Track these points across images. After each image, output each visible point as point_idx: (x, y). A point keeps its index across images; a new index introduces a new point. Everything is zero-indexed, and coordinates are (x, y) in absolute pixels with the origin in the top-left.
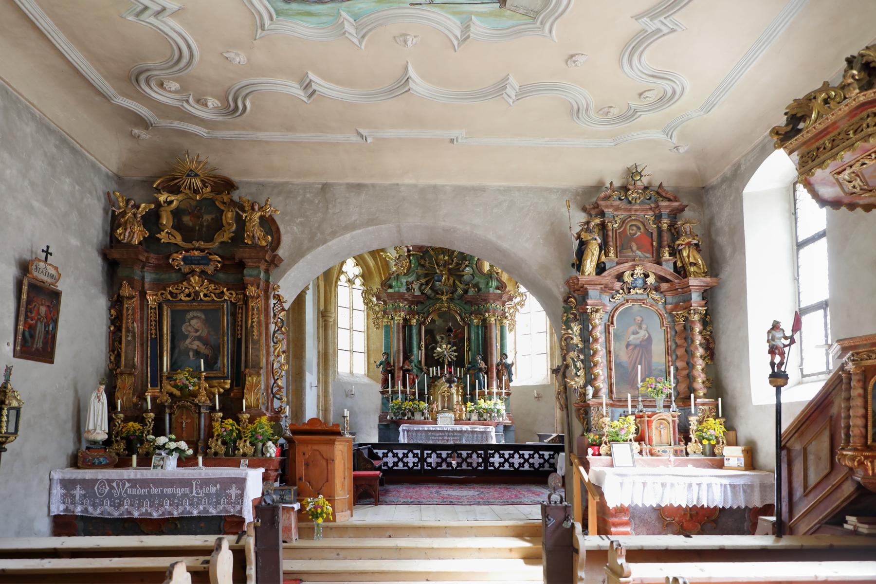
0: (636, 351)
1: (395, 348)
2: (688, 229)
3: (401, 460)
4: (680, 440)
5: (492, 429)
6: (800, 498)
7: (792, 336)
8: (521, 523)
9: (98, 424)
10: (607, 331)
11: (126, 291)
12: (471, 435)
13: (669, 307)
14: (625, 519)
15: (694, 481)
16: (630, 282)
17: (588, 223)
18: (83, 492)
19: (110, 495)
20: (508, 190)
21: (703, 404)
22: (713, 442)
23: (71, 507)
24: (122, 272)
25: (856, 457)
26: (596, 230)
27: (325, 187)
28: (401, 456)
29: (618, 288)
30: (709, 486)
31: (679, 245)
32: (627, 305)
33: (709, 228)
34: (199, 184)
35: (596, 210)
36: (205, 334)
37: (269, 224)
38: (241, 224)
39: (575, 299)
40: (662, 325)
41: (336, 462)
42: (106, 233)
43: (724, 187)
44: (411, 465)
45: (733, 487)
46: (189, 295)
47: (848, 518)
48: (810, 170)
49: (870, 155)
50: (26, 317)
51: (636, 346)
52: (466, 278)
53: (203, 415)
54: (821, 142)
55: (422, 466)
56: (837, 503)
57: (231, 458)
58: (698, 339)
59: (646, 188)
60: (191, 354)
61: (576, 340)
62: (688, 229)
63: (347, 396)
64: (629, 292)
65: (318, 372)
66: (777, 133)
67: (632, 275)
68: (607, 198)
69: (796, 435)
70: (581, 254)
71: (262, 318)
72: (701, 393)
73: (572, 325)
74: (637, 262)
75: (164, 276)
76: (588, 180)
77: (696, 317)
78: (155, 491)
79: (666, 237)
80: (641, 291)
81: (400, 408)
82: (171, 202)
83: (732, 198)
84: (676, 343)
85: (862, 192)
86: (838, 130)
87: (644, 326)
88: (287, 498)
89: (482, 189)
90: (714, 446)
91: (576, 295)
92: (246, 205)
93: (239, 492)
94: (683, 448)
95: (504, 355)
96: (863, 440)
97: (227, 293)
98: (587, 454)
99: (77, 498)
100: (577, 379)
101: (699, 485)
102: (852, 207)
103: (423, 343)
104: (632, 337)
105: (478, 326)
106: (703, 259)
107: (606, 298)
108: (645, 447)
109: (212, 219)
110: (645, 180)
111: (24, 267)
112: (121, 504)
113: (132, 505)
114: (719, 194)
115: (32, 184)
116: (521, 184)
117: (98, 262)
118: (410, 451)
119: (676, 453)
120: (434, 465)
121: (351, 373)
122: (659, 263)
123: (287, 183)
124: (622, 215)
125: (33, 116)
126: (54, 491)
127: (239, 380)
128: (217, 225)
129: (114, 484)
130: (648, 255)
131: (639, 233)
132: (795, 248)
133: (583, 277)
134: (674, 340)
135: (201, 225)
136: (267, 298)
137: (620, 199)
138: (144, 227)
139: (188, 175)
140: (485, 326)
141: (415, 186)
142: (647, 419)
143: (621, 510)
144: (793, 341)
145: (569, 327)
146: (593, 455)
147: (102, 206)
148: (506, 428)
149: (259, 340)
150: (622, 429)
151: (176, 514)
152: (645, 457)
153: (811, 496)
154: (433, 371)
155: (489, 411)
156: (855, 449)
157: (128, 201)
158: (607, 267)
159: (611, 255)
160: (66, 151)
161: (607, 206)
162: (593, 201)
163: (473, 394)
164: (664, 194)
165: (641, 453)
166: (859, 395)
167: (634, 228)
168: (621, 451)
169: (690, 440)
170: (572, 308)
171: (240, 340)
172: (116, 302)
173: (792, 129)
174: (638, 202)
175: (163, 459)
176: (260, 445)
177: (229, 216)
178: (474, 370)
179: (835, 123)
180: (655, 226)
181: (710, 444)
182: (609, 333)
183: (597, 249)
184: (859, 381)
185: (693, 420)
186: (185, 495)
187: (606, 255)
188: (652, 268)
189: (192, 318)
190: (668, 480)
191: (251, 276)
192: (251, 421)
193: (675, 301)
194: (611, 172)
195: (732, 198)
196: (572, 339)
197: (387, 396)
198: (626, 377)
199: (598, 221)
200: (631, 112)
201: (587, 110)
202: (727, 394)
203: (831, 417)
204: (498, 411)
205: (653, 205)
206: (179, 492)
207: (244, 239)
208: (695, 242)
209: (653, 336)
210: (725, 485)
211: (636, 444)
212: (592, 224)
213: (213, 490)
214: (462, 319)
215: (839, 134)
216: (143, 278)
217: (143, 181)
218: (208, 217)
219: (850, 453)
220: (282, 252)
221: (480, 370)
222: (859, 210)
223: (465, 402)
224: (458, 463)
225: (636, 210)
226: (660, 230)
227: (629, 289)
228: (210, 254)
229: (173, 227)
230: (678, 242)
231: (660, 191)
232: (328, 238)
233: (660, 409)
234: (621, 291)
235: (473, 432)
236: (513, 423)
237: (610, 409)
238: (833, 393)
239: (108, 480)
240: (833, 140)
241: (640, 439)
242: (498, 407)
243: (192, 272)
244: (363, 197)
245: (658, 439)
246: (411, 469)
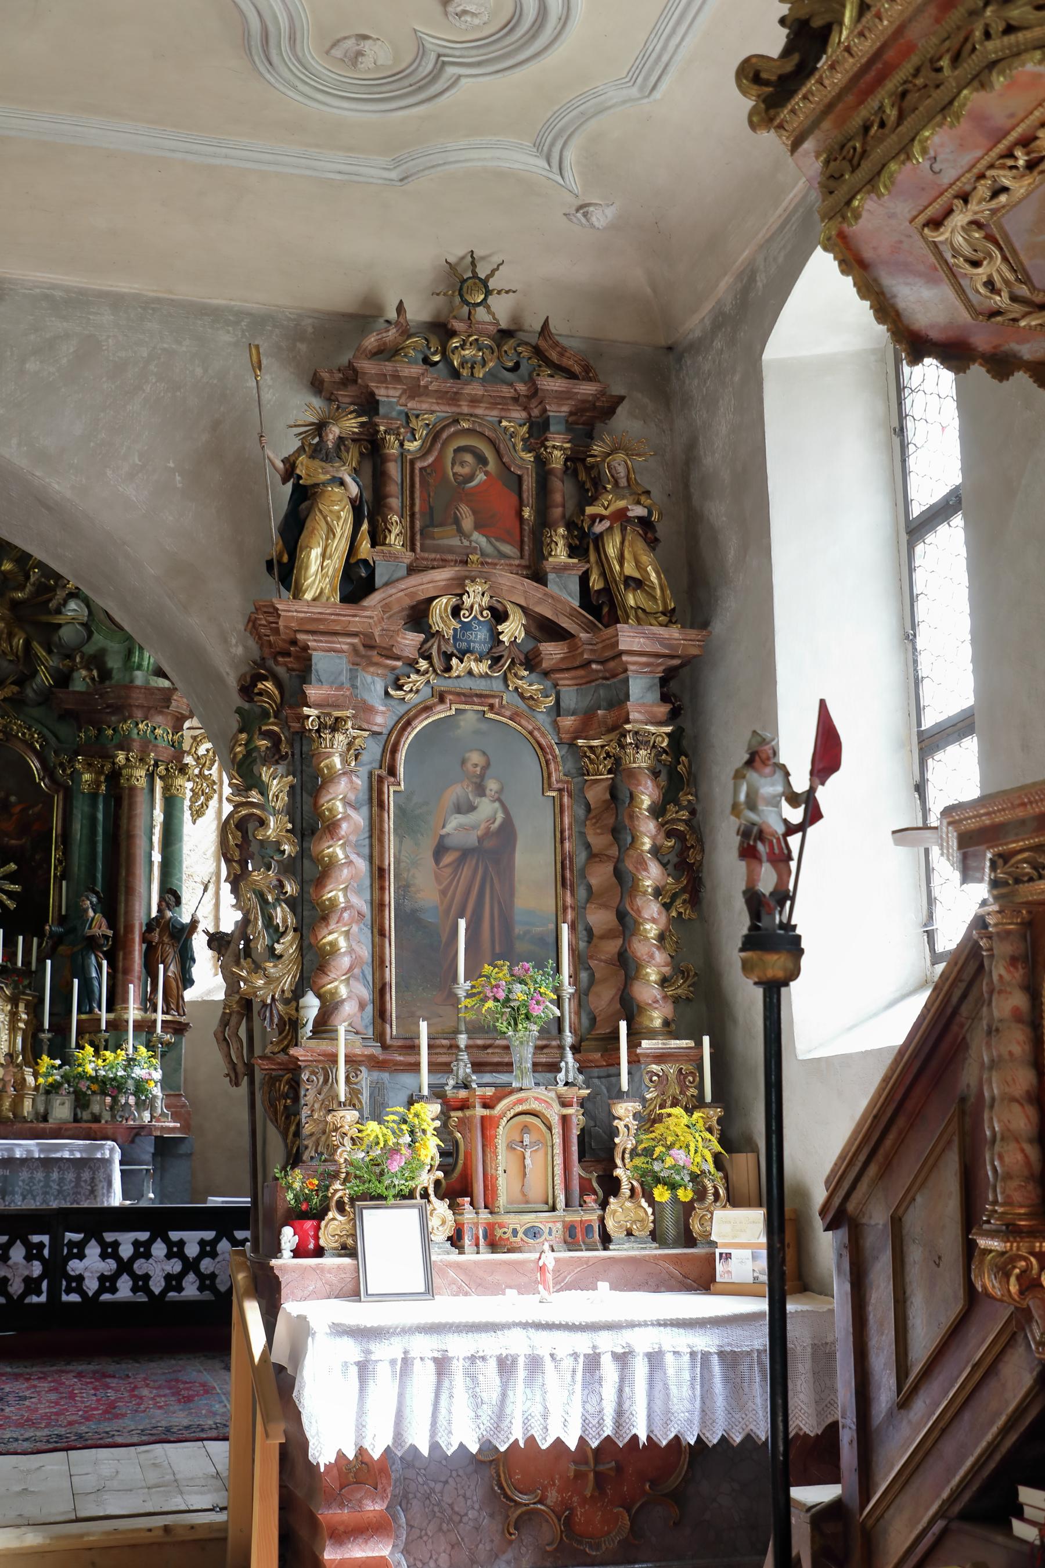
0: (466, 872)
2: (622, 471)
4: (586, 1189)
5: (111, 1151)
6: (890, 1414)
7: (812, 790)
8: (32, 1539)
10: (376, 800)
12: (39, 1175)
13: (568, 722)
14: (374, 1507)
15: (607, 1343)
16: (449, 633)
17: (320, 428)
20: (77, 302)
21: (661, 1058)
22: (685, 1195)
25: (1014, 1259)
26: (352, 456)
29: (411, 653)
30: (655, 1359)
31: (594, 518)
32: (441, 712)
33: (685, 475)
35: (352, 390)
39: (279, 685)
40: (547, 783)
43: (718, 344)
45: (730, 1359)
47: (1027, 1495)
48: (849, 203)
49: (1010, 155)
51: (465, 853)
52: (67, 634)
54: (873, 103)
56: (989, 1437)
58: (648, 833)
59: (505, 334)
61: (275, 827)
62: (622, 471)
64: (448, 669)
66: (757, 79)
67: (456, 611)
68: (387, 352)
69: (872, 1170)
70: (294, 528)
72: (656, 1019)
73: (265, 773)
74: (474, 568)
76: (331, 292)
77: (641, 759)
79: (561, 491)
80: (483, 667)
83: (737, 378)
84: (588, 846)
85: (1017, 309)
86: (915, 60)
87: (492, 786)
90: (688, 1209)
91: (281, 671)
94: (593, 1217)
95: (171, 896)
98: (276, 1250)
101: (623, 1359)
102: (1002, 365)
104: (454, 822)
105: (94, 796)
106: (665, 569)
107: (373, 686)
114: (707, 367)
116: (124, 286)
119: (572, 1238)
122: (539, 577)
124: (431, 411)
130: (507, 549)
131: (481, 477)
132: (904, 537)
133: (296, 606)
134: (582, 835)
137: (426, 361)
140: (118, 798)
142: (480, 1111)
143: (360, 1472)
144: (814, 814)
146: (298, 1252)
148: (165, 1148)
150: (395, 1151)
152: (469, 1257)
153: (920, 1405)
156: (1011, 1231)
158: (379, 581)
159: (392, 538)
161: (382, 378)
162: (345, 357)
163: (60, 1027)
164: (554, 356)
165: (455, 1240)
166: (1017, 1016)
167: (469, 458)
168: (392, 1237)
169: (612, 1187)
170: (265, 714)
174: (480, 373)
178: (72, 949)
179: (900, 31)
180: (529, 457)
181: (675, 1199)
182: (381, 805)
183: (346, 515)
184: (1014, 961)
185: (625, 1111)
187: (377, 539)
188: (515, 587)
190: (517, 1344)
193: (585, 703)
194: (397, 264)
195: (737, 378)
196: (262, 823)
198: (417, 957)
199: (351, 424)
200: (429, 65)
201: (292, 39)
202: (735, 1021)
203: (963, 1100)
204: (140, 1087)
205: (522, 388)
208: (639, 511)
209: (517, 823)
210: (706, 1356)
211: (441, 1207)
212: (333, 432)
214: (48, 770)
215: (917, 72)
219: (995, 1244)
221: (92, 944)
222: (1021, 379)
225: (474, 401)
226: (541, 463)
227: (448, 657)
230: (590, 510)
231: (543, 344)
233: (523, 1078)
234: (423, 664)
235: (47, 1163)
236: (186, 1127)
237: (365, 1078)
238: (964, 1010)
240: (904, 95)
241: (456, 1187)
242: (138, 1072)
245: (517, 1187)
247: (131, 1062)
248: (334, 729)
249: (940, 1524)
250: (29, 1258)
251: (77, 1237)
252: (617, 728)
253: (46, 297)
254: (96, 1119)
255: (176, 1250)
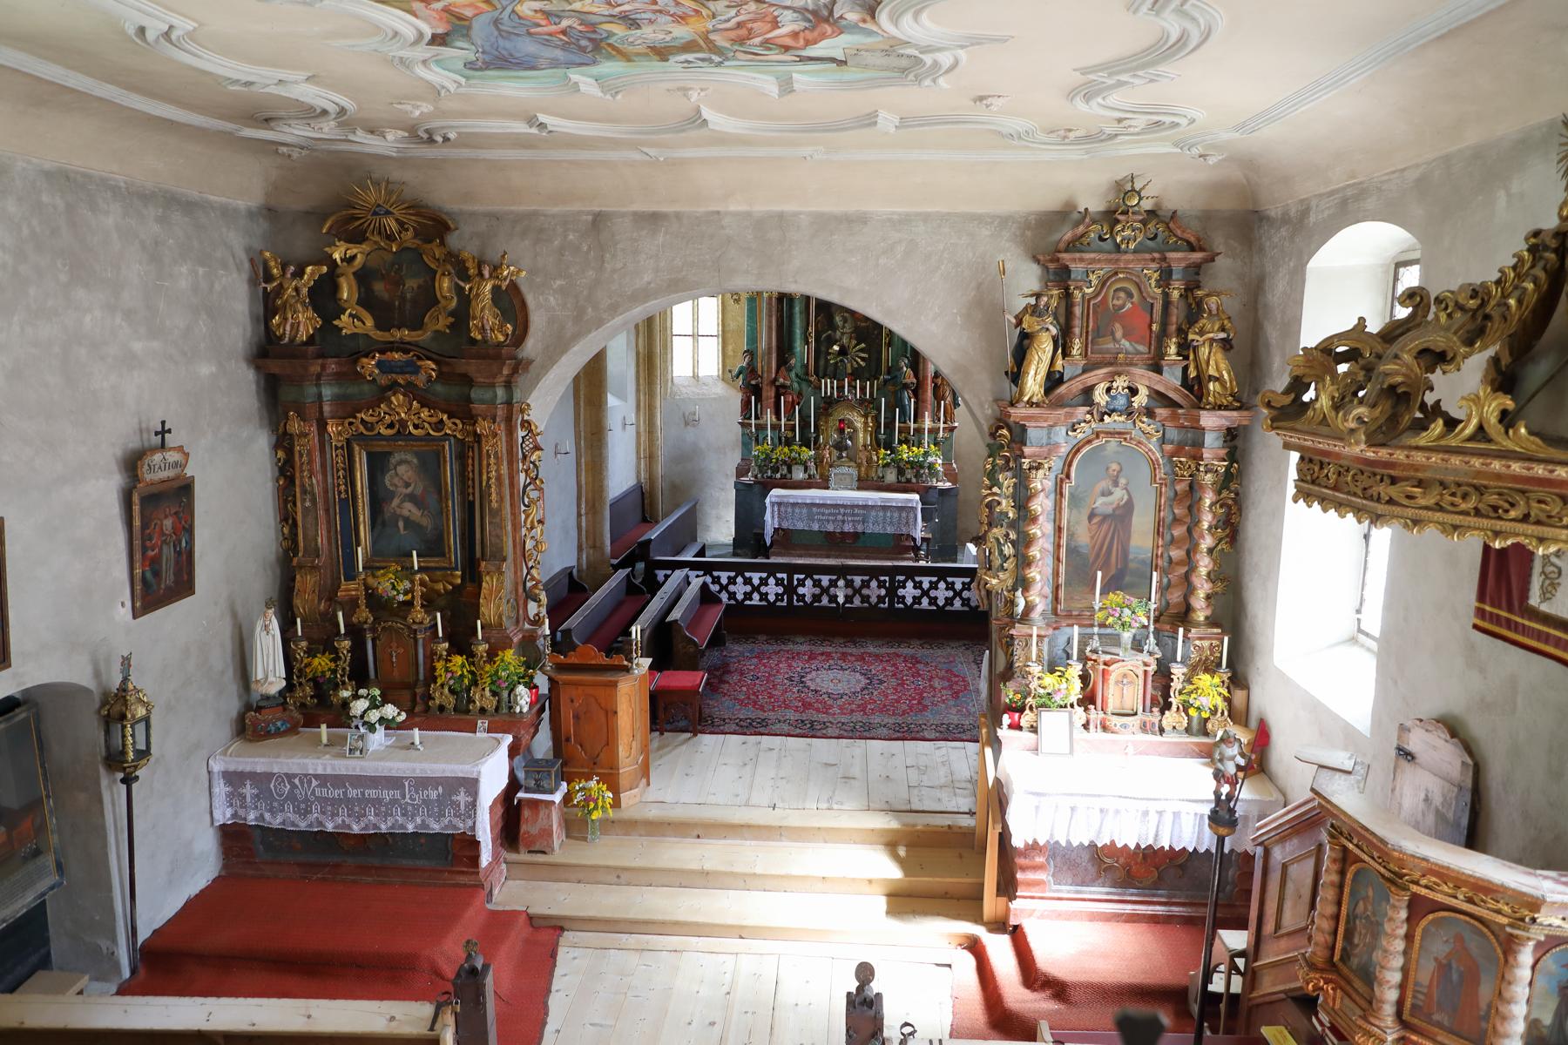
0: (1105, 527)
1: (763, 344)
2: (1214, 307)
3: (756, 589)
4: (1154, 702)
9: (270, 671)
11: (295, 426)
13: (1168, 447)
14: (1040, 860)
15: (1153, 807)
16: (1103, 403)
18: (255, 791)
19: (292, 797)
20: (905, 220)
22: (1205, 715)
23: (241, 812)
24: (287, 393)
27: (599, 221)
28: (756, 582)
30: (1176, 815)
32: (1096, 443)
34: (394, 225)
36: (419, 491)
37: (512, 304)
38: (465, 300)
39: (1010, 430)
41: (620, 713)
42: (258, 320)
44: (772, 598)
46: (391, 426)
50: (144, 549)
51: (1105, 517)
53: (420, 642)
55: (790, 600)
57: (459, 716)
59: (1152, 213)
60: (401, 524)
61: (1006, 505)
62: (1214, 307)
63: (687, 424)
65: (638, 390)
71: (504, 470)
75: (353, 390)
76: (1045, 199)
78: (353, 793)
80: (1122, 418)
81: (768, 458)
82: (354, 257)
87: (1122, 481)
88: (545, 784)
89: (862, 219)
90: (1206, 720)
92: (469, 264)
93: (470, 799)
94: (1156, 721)
96: (1327, 953)
97: (449, 423)
99: (248, 799)
100: (1001, 575)
101: (1160, 813)
103: (812, 329)
104: (1101, 500)
106: (1233, 367)
108: (1095, 715)
109: (419, 287)
110: (1147, 205)
111: (132, 463)
112: (307, 812)
113: (323, 813)
115: (128, 314)
117: (247, 377)
118: (772, 574)
120: (808, 599)
121: (695, 377)
122: (1157, 369)
123: (535, 214)
125: (115, 190)
126: (216, 790)
127: (473, 574)
128: (429, 299)
129: (297, 781)
130: (1141, 348)
131: (1129, 305)
135: (403, 298)
136: (510, 432)
138: (315, 310)
139: (375, 213)
141: (748, 214)
142: (1102, 667)
143: (1034, 847)
145: (995, 482)
146: (1011, 727)
147: (245, 276)
149: (500, 510)
151: (384, 828)
154: (828, 386)
155: (916, 466)
157: (284, 267)
158: (1066, 378)
160: (177, 217)
161: (1074, 260)
162: (1059, 241)
164: (1179, 233)
165: (1086, 726)
166: (1332, 884)
167: (1122, 295)
168: (1052, 721)
169: (1168, 706)
170: (1002, 446)
171: (472, 504)
172: (283, 442)
173: (1294, 401)
175: (362, 737)
176: (505, 694)
177: (445, 285)
185: (1178, 671)
186: (394, 802)
189: (401, 463)
191: (482, 402)
192: (492, 655)
196: (999, 503)
197: (751, 437)
206: (387, 795)
207: (469, 330)
210: (1202, 816)
211: (1079, 710)
213: (434, 795)
216: (320, 395)
217: (307, 213)
218: (412, 284)
220: (532, 347)
221: (906, 386)
223: (877, 444)
224: (846, 596)
225: (1128, 262)
226: (1166, 295)
228: (420, 358)
229: (360, 302)
232: (605, 316)
239: (286, 775)
241: (1088, 700)
242: (930, 459)
243: (393, 387)
244: (661, 238)
246: (772, 605)
247: (926, 454)
248: (1037, 469)
249: (1283, 996)
250: (879, 587)
251: (902, 578)
252: (1198, 458)
253: (889, 220)
254: (909, 481)
255: (748, 581)
